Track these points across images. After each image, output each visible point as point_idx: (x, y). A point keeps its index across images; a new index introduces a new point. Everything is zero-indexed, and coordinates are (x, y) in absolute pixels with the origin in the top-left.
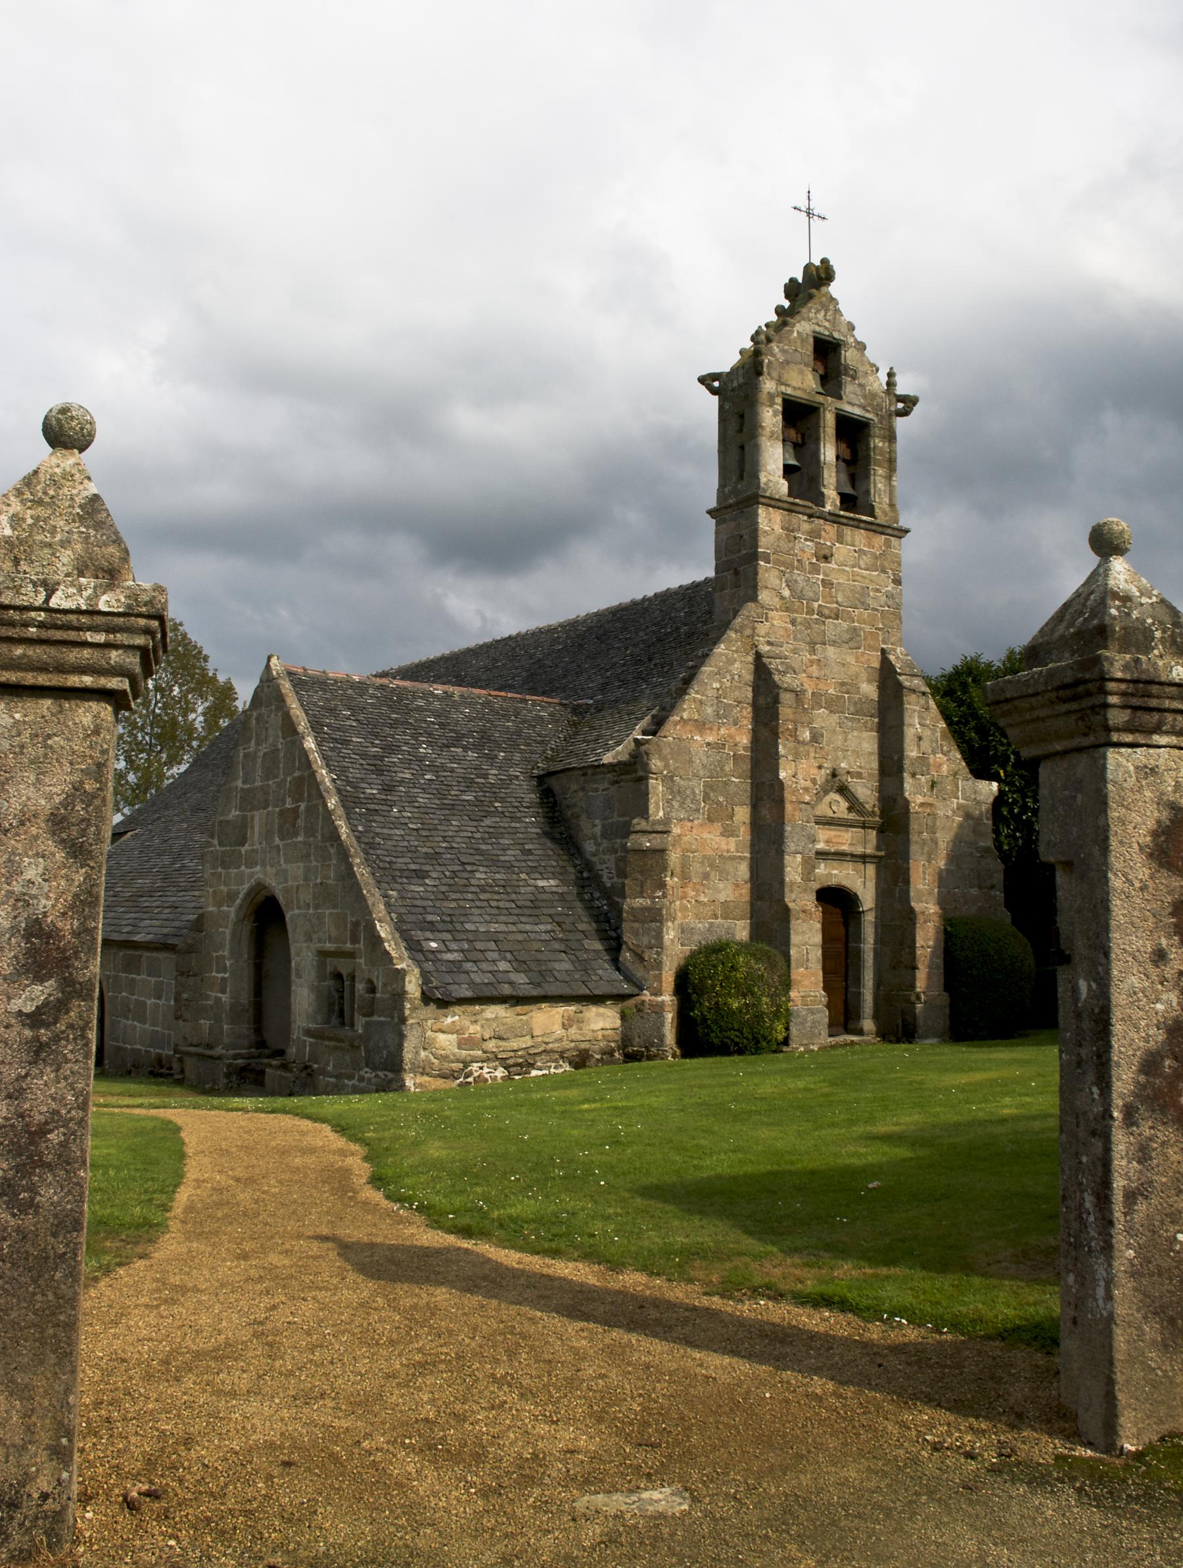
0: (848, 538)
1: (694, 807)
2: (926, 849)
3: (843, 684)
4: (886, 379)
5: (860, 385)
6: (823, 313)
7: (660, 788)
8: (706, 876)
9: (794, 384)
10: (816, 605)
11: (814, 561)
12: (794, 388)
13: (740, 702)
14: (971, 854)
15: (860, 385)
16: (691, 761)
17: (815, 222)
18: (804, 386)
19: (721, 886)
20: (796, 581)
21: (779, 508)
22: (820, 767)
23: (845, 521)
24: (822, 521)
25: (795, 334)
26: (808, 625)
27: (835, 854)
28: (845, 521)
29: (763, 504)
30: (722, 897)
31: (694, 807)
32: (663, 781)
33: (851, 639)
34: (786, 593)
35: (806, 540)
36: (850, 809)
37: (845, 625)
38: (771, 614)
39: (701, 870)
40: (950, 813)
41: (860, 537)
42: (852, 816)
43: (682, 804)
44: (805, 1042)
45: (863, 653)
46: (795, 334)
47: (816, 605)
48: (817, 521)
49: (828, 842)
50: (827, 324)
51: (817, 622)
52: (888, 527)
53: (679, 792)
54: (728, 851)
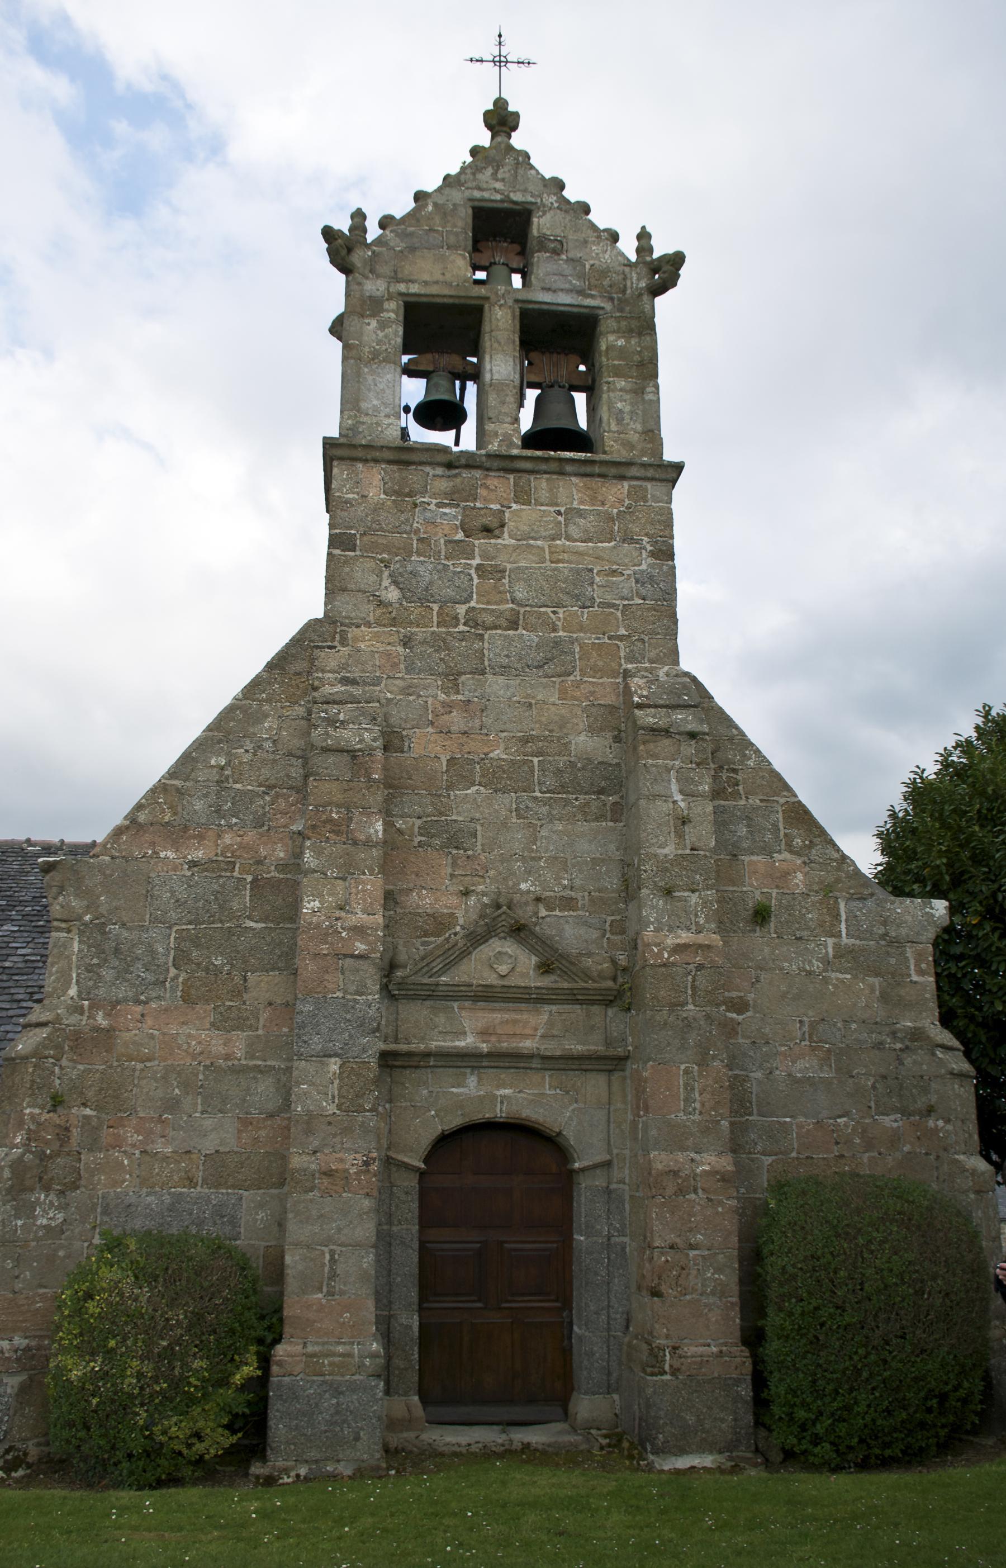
0: (544, 494)
1: (150, 977)
2: (692, 1039)
3: (525, 740)
4: (635, 244)
5: (570, 260)
6: (490, 171)
7: (76, 946)
8: (172, 1105)
9: (426, 277)
10: (462, 609)
11: (460, 536)
12: (426, 283)
13: (271, 787)
14: (879, 1046)
15: (570, 260)
16: (149, 895)
17: (490, 51)
18: (448, 277)
19: (208, 1123)
20: (414, 574)
21: (376, 461)
22: (466, 893)
23: (528, 465)
24: (478, 473)
25: (430, 208)
26: (440, 643)
27: (490, 1055)
28: (528, 465)
29: (341, 459)
30: (209, 1145)
31: (150, 977)
32: (81, 933)
33: (547, 661)
34: (393, 595)
35: (439, 505)
36: (545, 968)
37: (532, 638)
38: (352, 632)
39: (160, 1093)
40: (817, 965)
41: (572, 491)
42: (546, 981)
43: (122, 974)
44: (313, 1454)
45: (577, 685)
46: (430, 208)
47: (462, 609)
48: (466, 474)
49: (484, 1033)
50: (498, 185)
51: (463, 637)
52: (629, 464)
53: (117, 951)
54: (227, 1057)
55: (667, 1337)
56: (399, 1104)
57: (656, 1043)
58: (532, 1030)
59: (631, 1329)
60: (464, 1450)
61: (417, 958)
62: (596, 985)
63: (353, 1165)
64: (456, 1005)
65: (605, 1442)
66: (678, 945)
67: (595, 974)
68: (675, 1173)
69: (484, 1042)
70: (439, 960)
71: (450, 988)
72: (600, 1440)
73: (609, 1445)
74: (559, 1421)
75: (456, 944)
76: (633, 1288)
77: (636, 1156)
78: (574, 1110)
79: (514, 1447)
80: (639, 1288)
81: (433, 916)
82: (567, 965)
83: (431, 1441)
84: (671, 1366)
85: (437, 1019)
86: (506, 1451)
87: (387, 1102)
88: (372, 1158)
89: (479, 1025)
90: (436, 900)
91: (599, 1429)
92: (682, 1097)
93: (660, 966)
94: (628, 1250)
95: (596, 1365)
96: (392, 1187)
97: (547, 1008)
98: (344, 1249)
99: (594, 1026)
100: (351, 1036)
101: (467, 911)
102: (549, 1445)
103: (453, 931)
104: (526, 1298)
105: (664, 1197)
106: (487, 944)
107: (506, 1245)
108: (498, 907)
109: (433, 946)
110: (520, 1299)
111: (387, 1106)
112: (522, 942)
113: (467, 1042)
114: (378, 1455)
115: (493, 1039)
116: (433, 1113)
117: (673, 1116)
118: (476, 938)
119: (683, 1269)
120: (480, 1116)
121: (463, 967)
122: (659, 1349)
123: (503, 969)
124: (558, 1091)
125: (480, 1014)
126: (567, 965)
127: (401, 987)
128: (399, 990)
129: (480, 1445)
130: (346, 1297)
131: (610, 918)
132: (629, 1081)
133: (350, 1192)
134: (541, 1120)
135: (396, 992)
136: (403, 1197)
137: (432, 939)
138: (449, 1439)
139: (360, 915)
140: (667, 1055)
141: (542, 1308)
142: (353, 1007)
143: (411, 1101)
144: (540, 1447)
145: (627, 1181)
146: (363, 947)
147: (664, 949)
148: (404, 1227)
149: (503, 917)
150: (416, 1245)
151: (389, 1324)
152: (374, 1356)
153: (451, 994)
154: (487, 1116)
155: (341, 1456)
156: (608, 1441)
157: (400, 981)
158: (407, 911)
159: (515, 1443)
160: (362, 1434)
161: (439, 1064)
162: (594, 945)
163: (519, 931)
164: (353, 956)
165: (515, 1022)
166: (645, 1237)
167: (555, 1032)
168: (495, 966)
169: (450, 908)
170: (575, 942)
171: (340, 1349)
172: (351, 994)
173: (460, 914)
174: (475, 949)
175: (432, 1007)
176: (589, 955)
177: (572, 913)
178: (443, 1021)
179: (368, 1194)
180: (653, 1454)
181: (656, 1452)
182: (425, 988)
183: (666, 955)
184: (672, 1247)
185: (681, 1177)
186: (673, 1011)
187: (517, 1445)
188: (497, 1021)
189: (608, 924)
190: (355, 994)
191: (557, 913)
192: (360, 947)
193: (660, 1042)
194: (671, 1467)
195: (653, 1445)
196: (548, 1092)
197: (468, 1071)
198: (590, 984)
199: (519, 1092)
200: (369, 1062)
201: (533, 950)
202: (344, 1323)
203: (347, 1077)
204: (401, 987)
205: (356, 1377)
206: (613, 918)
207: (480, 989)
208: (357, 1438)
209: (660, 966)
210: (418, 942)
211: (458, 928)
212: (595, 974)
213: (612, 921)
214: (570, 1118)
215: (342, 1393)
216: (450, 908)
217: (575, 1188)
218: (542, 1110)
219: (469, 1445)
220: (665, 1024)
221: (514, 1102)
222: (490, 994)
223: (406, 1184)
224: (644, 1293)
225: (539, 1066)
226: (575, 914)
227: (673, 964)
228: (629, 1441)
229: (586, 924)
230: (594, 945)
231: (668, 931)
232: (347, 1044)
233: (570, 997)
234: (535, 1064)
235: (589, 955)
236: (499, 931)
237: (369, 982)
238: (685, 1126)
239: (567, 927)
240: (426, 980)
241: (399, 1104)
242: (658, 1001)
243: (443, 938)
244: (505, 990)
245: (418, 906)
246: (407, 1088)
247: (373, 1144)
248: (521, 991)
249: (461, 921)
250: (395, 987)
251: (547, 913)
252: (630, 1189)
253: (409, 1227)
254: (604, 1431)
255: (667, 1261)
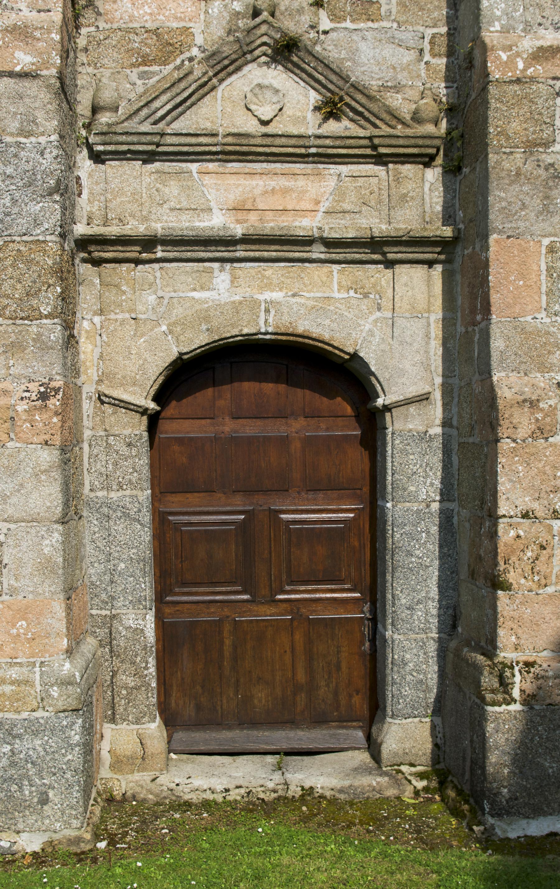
27: (246, 240)
36: (331, 109)
55: (516, 647)
56: (113, 316)
57: (504, 204)
58: (313, 199)
59: (460, 629)
60: (219, 798)
61: (133, 96)
62: (409, 132)
63: (22, 399)
64: (194, 167)
65: (421, 784)
66: (541, 48)
67: (408, 117)
68: (533, 404)
69: (238, 221)
70: (164, 98)
71: (183, 140)
72: (414, 782)
73: (426, 789)
74: (359, 749)
75: (190, 73)
76: (464, 573)
77: (469, 384)
78: (376, 321)
79: (290, 794)
80: (472, 574)
81: (155, 32)
82: (364, 100)
83: (173, 786)
84: (522, 691)
85: (167, 190)
86: (279, 798)
87: (95, 314)
88: (54, 389)
89: (232, 197)
90: (159, 8)
91: (412, 765)
92: (544, 289)
93: (511, 82)
94: (455, 520)
95: (409, 678)
96: (107, 436)
97: (334, 169)
98: (12, 526)
99: (405, 195)
100: (14, 201)
101: (207, 25)
102: (341, 791)
103: (187, 55)
104: (310, 587)
105: (514, 441)
106: (240, 74)
107: (282, 516)
108: (256, 13)
109: (156, 78)
110: (303, 588)
111: (97, 319)
112: (294, 68)
113: (216, 222)
114: (76, 823)
115: (253, 217)
116: (164, 328)
117: (529, 318)
118: (224, 64)
119: (543, 548)
120: (235, 332)
121: (204, 110)
122: (504, 665)
123: (266, 112)
124: (352, 293)
125: (232, 180)
126: (364, 100)
127: (107, 138)
128: (104, 144)
129: (242, 791)
130: (20, 597)
131: (430, 32)
132: (458, 277)
133: (19, 439)
134: (326, 336)
135: (100, 148)
136: (124, 450)
137: (155, 68)
138: (199, 782)
139: (26, 12)
140: (521, 224)
141: (335, 599)
142: (16, 156)
143: (130, 311)
144: (328, 794)
145: (455, 423)
146: (28, 59)
147: (518, 55)
148: (128, 492)
149: (264, 28)
150: (147, 518)
151: (110, 628)
152: (67, 682)
153: (185, 149)
154: (246, 331)
155: (21, 826)
156: (424, 783)
157: (105, 129)
158: (115, 26)
159: (292, 788)
160: (51, 794)
161: (171, 255)
162: (405, 74)
163: (286, 51)
164: (11, 74)
165: (285, 191)
166: (483, 502)
167: (346, 206)
168: (252, 107)
169: (181, 19)
170: (376, 69)
171: (14, 673)
172: (12, 134)
173: (197, 28)
174: (221, 81)
175: (157, 172)
176: (397, 88)
177: (370, 24)
178: (176, 192)
179: (46, 443)
180: (493, 816)
181: (498, 813)
182: (144, 139)
183: (521, 65)
184: (525, 516)
185: (542, 410)
186: (531, 153)
187: (295, 791)
188: (258, 191)
189: (427, 40)
190: (19, 135)
191: (348, 24)
192: (23, 59)
193: (510, 203)
194: (521, 834)
195: (493, 803)
196: (337, 295)
197: (216, 265)
198: (400, 130)
199: (294, 295)
200: (44, 242)
201: (312, 80)
202: (18, 635)
203: (12, 266)
204: (107, 138)
205: (39, 714)
206: (435, 30)
207: (230, 140)
208: (44, 801)
209: (511, 82)
210: (134, 75)
211: (195, 51)
212: (408, 117)
213: (434, 36)
214: (371, 333)
215: (19, 736)
216: (181, 19)
217: (379, 435)
218: (327, 322)
219: (227, 790)
220: (518, 174)
221: (285, 310)
222: (245, 149)
223: (127, 432)
224: (481, 582)
225: (322, 256)
226: (376, 25)
227: (533, 80)
228: (455, 787)
229: (392, 40)
230: (405, 74)
231: (524, 30)
232: (7, 214)
233: (368, 151)
234: (318, 251)
235: (397, 88)
236: (257, 53)
237: (40, 116)
238: (548, 333)
239: (363, 46)
240: (146, 127)
241: (113, 316)
242: (508, 138)
243: (171, 66)
244: (268, 141)
245: (132, 18)
246: (124, 293)
247: (58, 368)
248: (293, 141)
249: (199, 40)
250: (98, 139)
251: (332, 25)
252: (460, 435)
253: (134, 492)
254: (420, 769)
255: (518, 537)
